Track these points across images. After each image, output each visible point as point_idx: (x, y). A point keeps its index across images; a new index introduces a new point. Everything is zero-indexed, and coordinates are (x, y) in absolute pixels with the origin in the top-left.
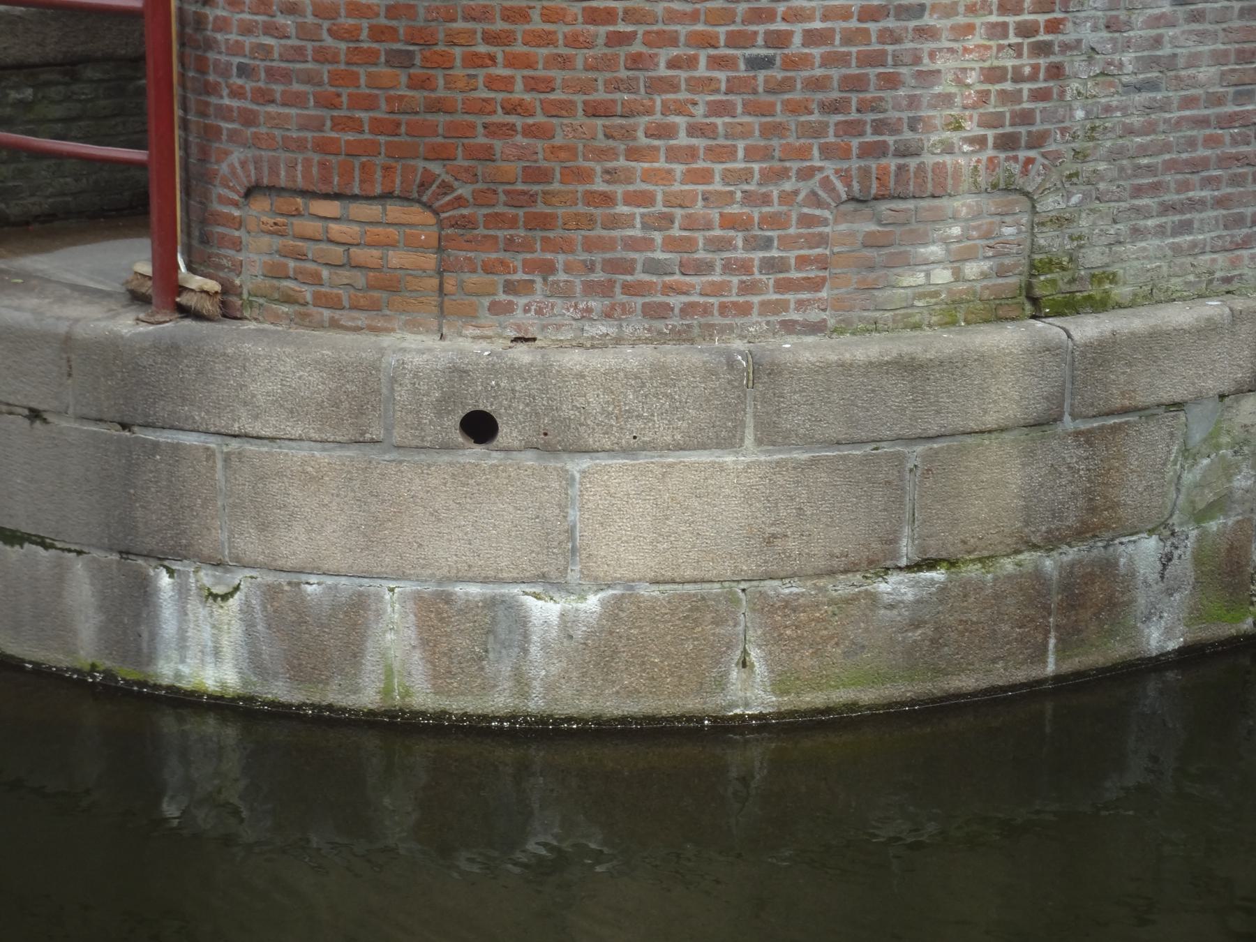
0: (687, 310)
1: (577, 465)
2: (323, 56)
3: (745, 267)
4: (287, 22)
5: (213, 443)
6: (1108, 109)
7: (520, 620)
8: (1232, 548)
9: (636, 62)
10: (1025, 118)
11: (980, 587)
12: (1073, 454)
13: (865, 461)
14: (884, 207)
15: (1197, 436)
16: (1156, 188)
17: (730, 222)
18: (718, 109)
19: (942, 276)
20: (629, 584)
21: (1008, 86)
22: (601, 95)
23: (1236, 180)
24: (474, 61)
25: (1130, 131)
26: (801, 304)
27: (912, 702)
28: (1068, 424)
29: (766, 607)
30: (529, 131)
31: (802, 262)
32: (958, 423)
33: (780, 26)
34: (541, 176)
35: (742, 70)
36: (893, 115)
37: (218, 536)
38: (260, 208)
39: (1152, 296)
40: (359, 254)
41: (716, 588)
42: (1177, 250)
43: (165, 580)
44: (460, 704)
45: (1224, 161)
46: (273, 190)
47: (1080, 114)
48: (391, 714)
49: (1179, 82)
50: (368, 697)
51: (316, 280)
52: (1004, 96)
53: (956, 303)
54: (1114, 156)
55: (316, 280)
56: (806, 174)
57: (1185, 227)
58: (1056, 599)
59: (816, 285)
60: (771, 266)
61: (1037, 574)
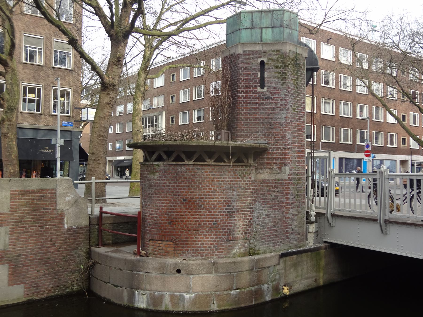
0: (206, 255)
1: (191, 276)
2: (160, 223)
3: (213, 250)
4: (156, 219)
5: (144, 273)
7: (183, 297)
9: (199, 224)
10: (248, 230)
11: (244, 292)
12: (256, 274)
14: (231, 242)
15: (271, 271)
16: (264, 239)
17: (211, 244)
18: (209, 230)
19: (238, 251)
20: (198, 292)
22: (195, 228)
23: (274, 238)
24: (179, 224)
25: (261, 232)
26: (220, 254)
27: (235, 308)
28: (255, 270)
30: (186, 232)
31: (220, 249)
32: (241, 270)
34: (187, 238)
36: (231, 230)
37: (144, 286)
38: (151, 242)
39: (265, 253)
41: (209, 293)
42: (267, 246)
43: (137, 292)
45: (273, 235)
46: (153, 240)
48: (166, 311)
49: (267, 225)
50: (163, 309)
51: (158, 252)
52: (245, 228)
54: (259, 235)
55: (158, 252)
56: (221, 238)
57: (268, 244)
59: (222, 252)
60: (216, 249)
61: (252, 290)
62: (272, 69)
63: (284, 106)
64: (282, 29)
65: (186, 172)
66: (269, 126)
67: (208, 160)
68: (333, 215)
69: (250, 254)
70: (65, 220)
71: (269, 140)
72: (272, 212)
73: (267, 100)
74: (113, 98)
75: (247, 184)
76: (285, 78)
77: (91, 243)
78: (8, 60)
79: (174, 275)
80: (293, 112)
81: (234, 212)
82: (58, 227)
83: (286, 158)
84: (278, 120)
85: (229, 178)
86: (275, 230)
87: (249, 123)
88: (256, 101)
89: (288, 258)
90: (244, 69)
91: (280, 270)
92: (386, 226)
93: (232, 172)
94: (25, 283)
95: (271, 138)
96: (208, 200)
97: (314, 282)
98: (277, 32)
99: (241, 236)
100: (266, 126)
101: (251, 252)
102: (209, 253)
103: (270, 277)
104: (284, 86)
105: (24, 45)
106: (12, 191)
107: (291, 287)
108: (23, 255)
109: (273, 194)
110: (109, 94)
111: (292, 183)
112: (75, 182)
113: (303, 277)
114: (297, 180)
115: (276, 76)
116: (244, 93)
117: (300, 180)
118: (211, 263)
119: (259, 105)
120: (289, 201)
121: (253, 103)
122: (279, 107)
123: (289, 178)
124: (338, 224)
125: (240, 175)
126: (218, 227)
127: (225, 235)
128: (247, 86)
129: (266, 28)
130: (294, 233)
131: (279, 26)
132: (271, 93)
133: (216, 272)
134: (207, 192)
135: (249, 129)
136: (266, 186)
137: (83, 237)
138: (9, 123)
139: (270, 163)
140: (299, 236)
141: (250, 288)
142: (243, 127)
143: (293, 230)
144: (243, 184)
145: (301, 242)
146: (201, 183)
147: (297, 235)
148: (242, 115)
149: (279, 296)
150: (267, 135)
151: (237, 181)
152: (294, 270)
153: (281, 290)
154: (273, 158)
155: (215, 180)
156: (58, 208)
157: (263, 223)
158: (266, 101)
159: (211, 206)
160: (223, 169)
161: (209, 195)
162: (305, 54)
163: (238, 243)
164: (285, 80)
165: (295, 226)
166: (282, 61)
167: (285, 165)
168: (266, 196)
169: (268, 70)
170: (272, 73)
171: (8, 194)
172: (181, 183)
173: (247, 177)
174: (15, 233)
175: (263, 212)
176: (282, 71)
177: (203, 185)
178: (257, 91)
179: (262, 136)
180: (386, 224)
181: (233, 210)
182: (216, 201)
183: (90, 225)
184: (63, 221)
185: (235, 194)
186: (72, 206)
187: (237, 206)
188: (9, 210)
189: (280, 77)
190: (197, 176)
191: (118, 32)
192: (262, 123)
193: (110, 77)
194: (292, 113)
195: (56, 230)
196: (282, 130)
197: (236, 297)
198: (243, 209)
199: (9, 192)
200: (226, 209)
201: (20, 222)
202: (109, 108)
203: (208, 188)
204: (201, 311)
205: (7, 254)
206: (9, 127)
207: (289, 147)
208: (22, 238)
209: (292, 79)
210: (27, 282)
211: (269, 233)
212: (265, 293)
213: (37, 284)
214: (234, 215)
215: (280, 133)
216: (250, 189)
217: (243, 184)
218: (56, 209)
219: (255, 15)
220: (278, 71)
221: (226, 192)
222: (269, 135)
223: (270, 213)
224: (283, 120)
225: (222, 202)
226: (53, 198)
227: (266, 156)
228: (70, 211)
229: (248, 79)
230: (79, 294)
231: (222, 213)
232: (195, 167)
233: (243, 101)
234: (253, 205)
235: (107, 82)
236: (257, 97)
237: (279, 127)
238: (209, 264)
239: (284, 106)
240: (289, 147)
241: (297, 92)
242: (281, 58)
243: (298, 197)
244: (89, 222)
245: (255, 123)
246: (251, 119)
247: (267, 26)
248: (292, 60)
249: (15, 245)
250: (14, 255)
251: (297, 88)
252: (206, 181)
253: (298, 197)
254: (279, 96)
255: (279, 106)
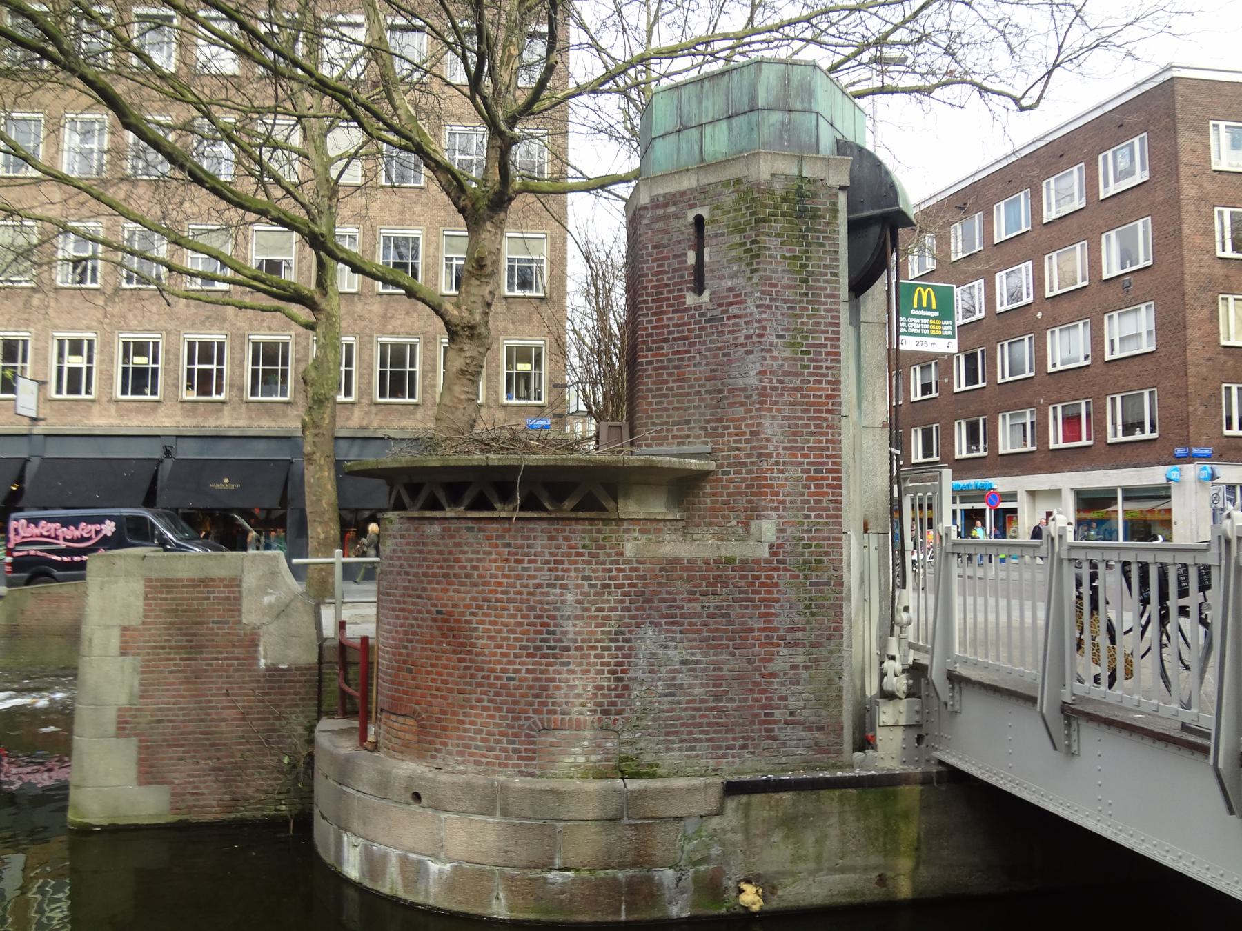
0: (488, 764)
1: (444, 815)
3: (506, 750)
6: (651, 702)
7: (427, 869)
8: (712, 878)
9: (472, 676)
10: (614, 704)
11: (589, 881)
12: (629, 833)
13: (540, 826)
14: (557, 732)
15: (690, 832)
16: (676, 733)
17: (502, 734)
18: (497, 694)
19: (581, 760)
20: (459, 861)
21: (605, 692)
22: (462, 687)
23: (716, 732)
24: (428, 673)
25: (662, 711)
26: (526, 766)
27: (562, 923)
28: (626, 820)
29: (505, 877)
30: (442, 697)
31: (527, 750)
32: (577, 816)
33: (517, 667)
34: (444, 712)
35: (505, 681)
36: (559, 700)
39: (676, 774)
40: (401, 734)
41: (487, 868)
42: (689, 757)
44: (411, 898)
45: (709, 724)
47: (638, 704)
48: (393, 897)
49: (685, 694)
50: (386, 890)
52: (603, 696)
53: (587, 770)
54: (655, 720)
56: (527, 719)
57: (693, 748)
58: (625, 890)
59: (533, 759)
60: (515, 751)
61: (615, 879)
62: (723, 235)
63: (756, 339)
64: (754, 115)
65: (443, 538)
66: (715, 402)
67: (498, 506)
68: (954, 679)
69: (625, 775)
70: (261, 649)
71: (717, 443)
72: (705, 655)
73: (712, 327)
74: (473, 358)
75: (610, 571)
76: (758, 256)
77: (324, 708)
78: (317, 297)
79: (407, 807)
80: (788, 354)
81: (568, 649)
82: (244, 665)
83: (761, 494)
84: (741, 382)
85: (551, 554)
86: (719, 710)
87: (666, 396)
88: (683, 331)
89: (757, 799)
90: (655, 247)
91: (725, 831)
92: (1069, 726)
93: (560, 539)
94: (172, 783)
95: (723, 435)
96: (493, 613)
97: (873, 886)
98: (741, 128)
99: (588, 718)
100: (709, 402)
101: (627, 768)
102: (496, 757)
103: (687, 848)
104: (755, 280)
105: (507, 256)
106: (148, 580)
107: (774, 887)
108: (169, 721)
109: (711, 602)
110: (461, 350)
111: (786, 570)
112: (295, 561)
113: (826, 865)
114: (805, 562)
115: (734, 253)
116: (653, 315)
117: (821, 561)
118: (492, 785)
119: (691, 345)
120: (775, 624)
121: (675, 339)
122: (742, 345)
123: (773, 554)
124: (973, 708)
125: (584, 547)
126: (520, 687)
127: (541, 713)
128: (661, 293)
129: (714, 121)
130: (799, 723)
131: (747, 109)
132: (720, 305)
133: (506, 813)
134: (491, 591)
135: (665, 414)
136: (681, 578)
137: (302, 691)
138: (316, 431)
139: (720, 510)
140: (818, 735)
141: (610, 871)
142: (653, 410)
143: (792, 714)
144: (594, 571)
145: (827, 752)
146: (475, 568)
147: (810, 729)
148: (649, 376)
149: (723, 911)
150: (712, 428)
151: (576, 562)
152: (786, 837)
153: (732, 894)
154: (729, 495)
155: (513, 558)
156: (245, 621)
157: (670, 686)
158: (709, 330)
159: (500, 631)
160: (532, 530)
161: (497, 601)
162: (839, 177)
163: (580, 738)
164: (758, 263)
165: (801, 703)
166: (747, 208)
167: (759, 517)
168: (683, 608)
169: (714, 242)
170: (724, 247)
171: (139, 586)
172: (432, 567)
173: (608, 551)
174: (153, 672)
175: (671, 653)
176: (750, 236)
177: (481, 571)
178: (684, 303)
179: (698, 432)
180: (1068, 718)
181: (565, 644)
182: (514, 616)
183: (320, 661)
184: (256, 651)
185: (569, 597)
186: (278, 616)
187: (576, 633)
188: (140, 621)
189: (743, 255)
190: (466, 549)
191: (478, 199)
192: (698, 393)
193: (464, 307)
194: (785, 359)
195: (238, 671)
196: (751, 411)
197: (562, 892)
198: (597, 641)
199: (142, 582)
200: (542, 640)
201: (163, 648)
202: (466, 381)
203: (493, 580)
204: (466, 914)
205: (135, 716)
206: (317, 439)
207: (771, 460)
208: (167, 684)
209: (784, 257)
210: (177, 782)
211: (693, 717)
212: (667, 895)
213: (197, 787)
214: (568, 657)
215: (744, 419)
216: (618, 586)
217: (594, 571)
218: (240, 622)
219: (685, 92)
220: (737, 238)
221: (542, 593)
222: (716, 428)
223: (699, 657)
224: (752, 381)
225: (532, 620)
226: (235, 598)
227: (708, 490)
228: (272, 628)
229: (663, 272)
230: (274, 824)
231: (531, 651)
232: (464, 524)
233: (650, 335)
234: (630, 632)
235: (456, 321)
236: (686, 320)
237: (742, 404)
238: (485, 788)
239: (756, 339)
240: (771, 460)
241: (807, 295)
242: (745, 201)
243: (812, 614)
244: (316, 656)
245: (681, 395)
246: (671, 384)
247: (717, 117)
248: (784, 200)
249: (151, 697)
250: (150, 718)
251: (805, 281)
252: (490, 561)
253: (812, 614)
254: (743, 312)
255: (742, 340)
